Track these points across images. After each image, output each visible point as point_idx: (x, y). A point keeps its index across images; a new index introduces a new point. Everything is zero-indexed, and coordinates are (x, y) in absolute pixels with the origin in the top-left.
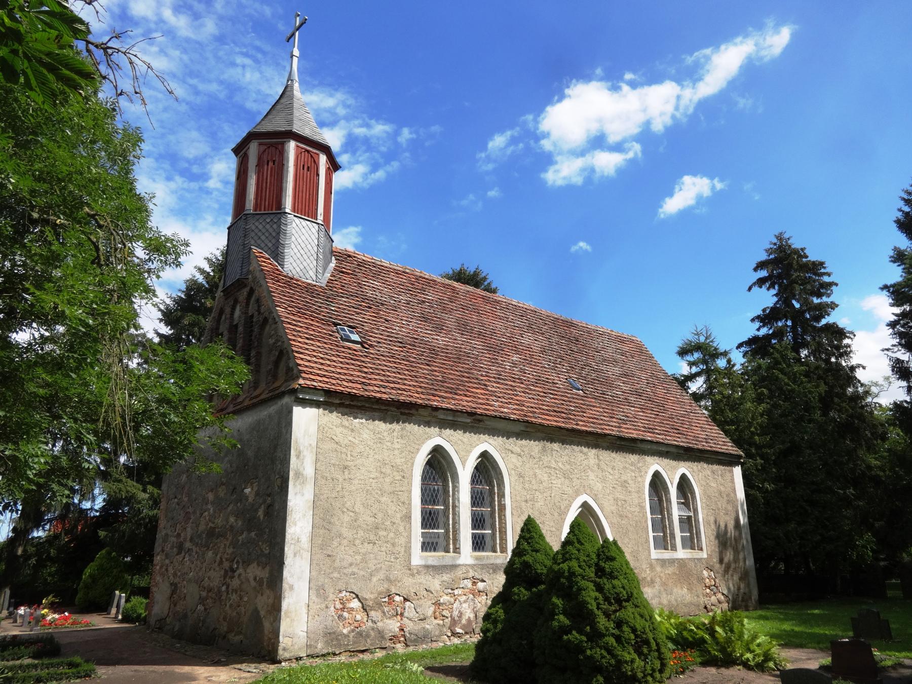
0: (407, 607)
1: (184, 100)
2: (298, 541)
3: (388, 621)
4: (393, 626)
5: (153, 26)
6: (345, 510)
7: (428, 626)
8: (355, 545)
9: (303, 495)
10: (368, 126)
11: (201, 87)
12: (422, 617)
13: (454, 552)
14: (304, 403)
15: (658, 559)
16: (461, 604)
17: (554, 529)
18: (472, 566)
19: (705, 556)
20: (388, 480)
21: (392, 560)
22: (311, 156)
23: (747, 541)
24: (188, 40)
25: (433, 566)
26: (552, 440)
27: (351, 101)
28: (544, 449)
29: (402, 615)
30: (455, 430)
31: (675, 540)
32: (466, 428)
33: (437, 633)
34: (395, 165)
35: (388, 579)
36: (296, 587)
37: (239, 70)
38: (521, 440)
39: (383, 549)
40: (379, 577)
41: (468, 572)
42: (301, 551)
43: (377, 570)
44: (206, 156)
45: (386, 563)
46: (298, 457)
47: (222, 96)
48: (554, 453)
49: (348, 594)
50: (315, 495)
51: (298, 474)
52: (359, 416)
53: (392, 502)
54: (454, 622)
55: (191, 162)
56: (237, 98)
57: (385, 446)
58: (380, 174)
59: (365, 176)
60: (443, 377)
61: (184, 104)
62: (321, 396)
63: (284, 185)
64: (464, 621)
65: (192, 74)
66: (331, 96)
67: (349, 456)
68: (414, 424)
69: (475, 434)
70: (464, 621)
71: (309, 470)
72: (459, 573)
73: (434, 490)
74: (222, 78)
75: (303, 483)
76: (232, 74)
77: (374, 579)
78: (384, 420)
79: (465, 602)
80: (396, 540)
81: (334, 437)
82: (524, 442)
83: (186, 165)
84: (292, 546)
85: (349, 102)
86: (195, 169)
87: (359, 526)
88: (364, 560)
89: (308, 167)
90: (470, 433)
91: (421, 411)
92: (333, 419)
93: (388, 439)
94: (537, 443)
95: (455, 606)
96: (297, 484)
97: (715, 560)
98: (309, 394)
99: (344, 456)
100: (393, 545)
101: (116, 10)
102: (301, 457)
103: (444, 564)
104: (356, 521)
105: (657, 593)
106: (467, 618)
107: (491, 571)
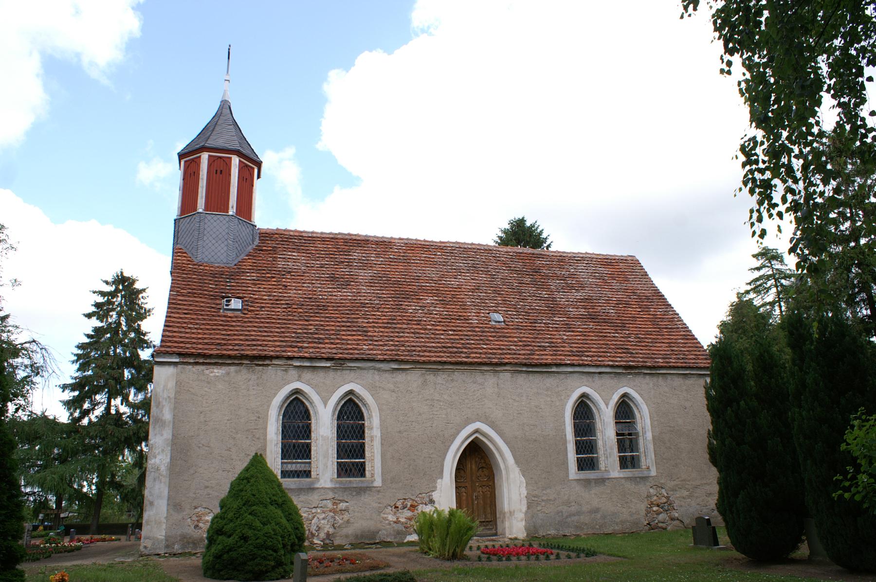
2: (158, 469)
9: (162, 435)
15: (579, 480)
22: (224, 160)
36: (156, 503)
42: (161, 477)
49: (203, 510)
50: (173, 435)
53: (247, 438)
57: (240, 394)
71: (167, 415)
73: (299, 427)
75: (162, 426)
79: (324, 519)
84: (153, 473)
89: (221, 171)
95: (313, 521)
96: (157, 426)
102: (160, 407)
104: (211, 454)
105: (235, 543)
106: (326, 532)
107: (354, 493)
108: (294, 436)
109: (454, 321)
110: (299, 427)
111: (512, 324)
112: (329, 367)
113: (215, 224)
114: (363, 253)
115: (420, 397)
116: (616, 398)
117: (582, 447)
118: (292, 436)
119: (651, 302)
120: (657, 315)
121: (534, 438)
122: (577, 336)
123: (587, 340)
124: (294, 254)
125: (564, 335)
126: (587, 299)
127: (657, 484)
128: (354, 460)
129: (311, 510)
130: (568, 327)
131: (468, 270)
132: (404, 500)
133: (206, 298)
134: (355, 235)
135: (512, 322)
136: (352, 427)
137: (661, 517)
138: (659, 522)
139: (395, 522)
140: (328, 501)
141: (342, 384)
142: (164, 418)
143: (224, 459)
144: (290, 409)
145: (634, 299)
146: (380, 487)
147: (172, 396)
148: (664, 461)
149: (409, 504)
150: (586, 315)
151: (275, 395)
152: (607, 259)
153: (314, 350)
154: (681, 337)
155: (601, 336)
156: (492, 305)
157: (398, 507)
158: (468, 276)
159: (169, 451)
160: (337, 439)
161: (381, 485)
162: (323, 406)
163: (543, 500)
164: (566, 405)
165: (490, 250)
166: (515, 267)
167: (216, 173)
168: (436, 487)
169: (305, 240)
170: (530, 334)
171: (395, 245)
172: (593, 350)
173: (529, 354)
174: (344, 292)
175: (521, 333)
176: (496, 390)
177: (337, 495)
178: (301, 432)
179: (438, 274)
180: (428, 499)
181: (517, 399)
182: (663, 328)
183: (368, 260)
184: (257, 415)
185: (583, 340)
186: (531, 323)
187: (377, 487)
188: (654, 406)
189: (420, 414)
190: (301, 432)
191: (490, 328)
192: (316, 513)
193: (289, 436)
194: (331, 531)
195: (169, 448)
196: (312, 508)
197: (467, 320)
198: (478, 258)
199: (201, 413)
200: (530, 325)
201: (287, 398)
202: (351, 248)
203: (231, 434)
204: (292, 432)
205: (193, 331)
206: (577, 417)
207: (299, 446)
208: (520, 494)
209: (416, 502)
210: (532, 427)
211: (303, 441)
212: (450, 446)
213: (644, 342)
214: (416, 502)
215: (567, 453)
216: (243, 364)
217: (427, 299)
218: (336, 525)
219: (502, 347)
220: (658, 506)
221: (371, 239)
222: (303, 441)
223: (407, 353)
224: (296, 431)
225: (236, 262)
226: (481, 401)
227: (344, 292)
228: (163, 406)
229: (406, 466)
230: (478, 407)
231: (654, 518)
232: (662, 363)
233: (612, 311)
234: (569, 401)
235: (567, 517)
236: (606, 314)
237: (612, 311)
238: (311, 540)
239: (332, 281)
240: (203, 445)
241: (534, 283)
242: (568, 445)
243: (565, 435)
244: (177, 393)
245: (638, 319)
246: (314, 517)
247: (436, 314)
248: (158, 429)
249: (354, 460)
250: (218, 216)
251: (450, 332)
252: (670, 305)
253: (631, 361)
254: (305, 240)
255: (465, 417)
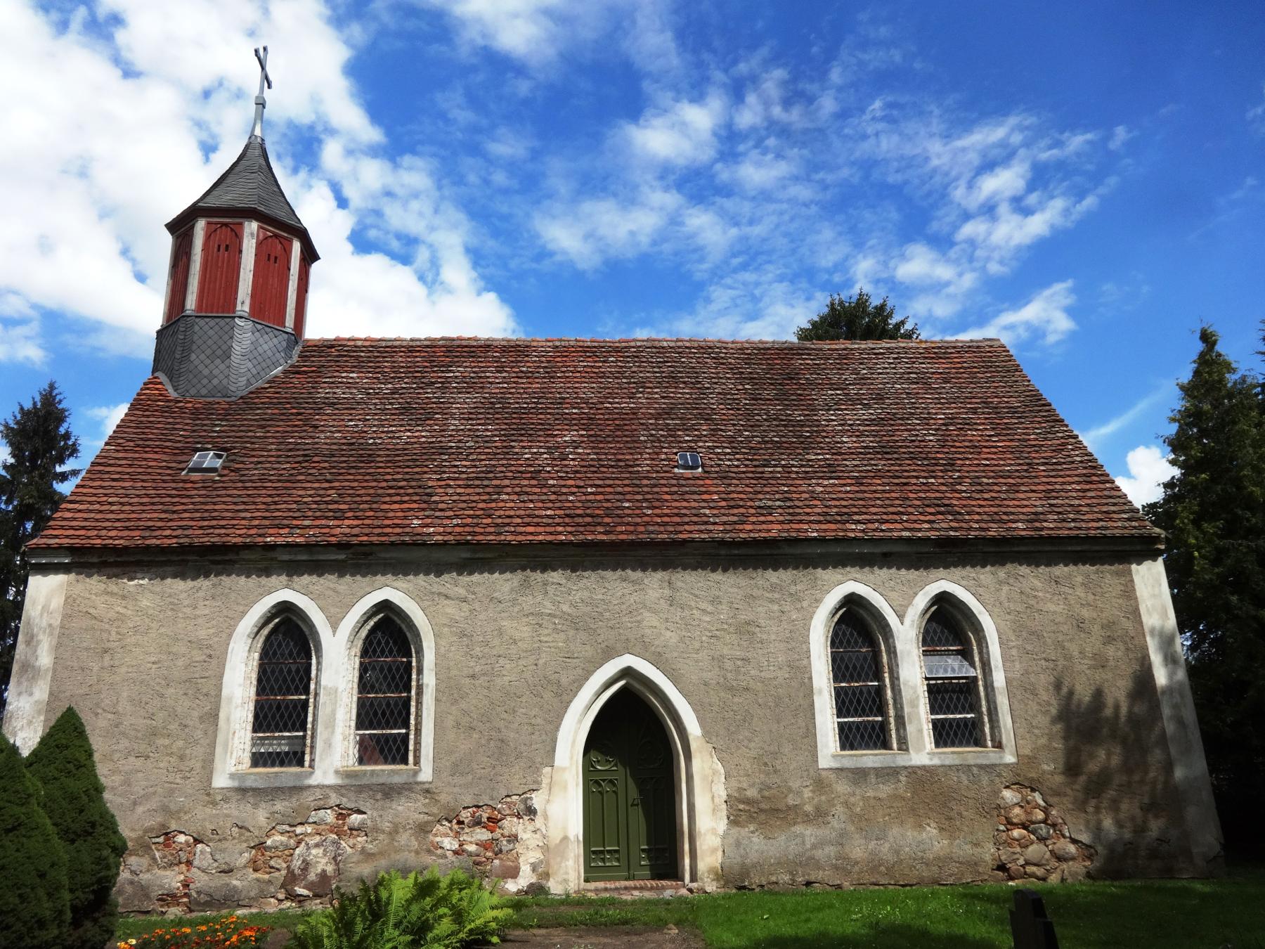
0: (198, 851)
1: (812, 202)
3: (161, 873)
4: (172, 879)
5: (763, 133)
6: (100, 711)
7: (235, 882)
8: (112, 760)
9: (31, 694)
10: (1058, 144)
11: (830, 178)
12: (224, 867)
13: (899, 749)
14: (44, 569)
15: (841, 770)
16: (308, 848)
17: (539, 721)
18: (336, 788)
19: (1010, 758)
20: (180, 663)
21: (178, 781)
22: (232, 230)
23: (1180, 722)
24: (806, 131)
25: (254, 790)
26: (545, 567)
27: (1031, 120)
28: (525, 584)
29: (189, 863)
30: (320, 575)
31: (905, 729)
32: (341, 569)
33: (252, 894)
34: (1113, 181)
35: (165, 809)
37: (872, 141)
38: (471, 573)
39: (161, 765)
40: (148, 806)
41: (327, 797)
43: (147, 797)
44: (846, 258)
45: (166, 785)
46: (28, 643)
47: (856, 180)
48: (551, 589)
50: (51, 694)
51: (26, 667)
52: (139, 575)
54: (291, 878)
55: (830, 272)
56: (876, 175)
57: (180, 615)
58: (1090, 202)
59: (1066, 212)
60: (339, 495)
61: (813, 206)
62: (66, 557)
63: (170, 282)
64: (312, 876)
65: (816, 168)
66: (1000, 124)
67: (113, 633)
68: (238, 575)
69: (364, 576)
70: (312, 876)
71: (45, 659)
72: (309, 799)
73: (289, 671)
74: (852, 158)
75: (33, 678)
76: (866, 147)
77: (140, 809)
78: (183, 576)
79: (317, 845)
80: (188, 752)
81: (91, 611)
82: (476, 577)
83: (826, 277)
85: (1027, 123)
86: (837, 278)
87: (124, 734)
88: (127, 783)
89: (227, 246)
90: (353, 575)
91: (246, 555)
92: (93, 588)
93: (186, 602)
94: (508, 575)
95: (298, 851)
96: (23, 680)
97: (1049, 767)
98: (44, 556)
99: (105, 636)
100: (182, 758)
101: (723, 133)
103: (277, 785)
104: (117, 726)
107: (379, 796)
108: (280, 689)
109: (605, 470)
110: (289, 671)
111: (717, 469)
112: (343, 561)
113: (211, 332)
114: (475, 367)
115: (516, 610)
116: (922, 600)
117: (851, 702)
118: (276, 688)
119: (1020, 417)
120: (1029, 440)
121: (744, 684)
122: (845, 485)
123: (865, 492)
124: (351, 375)
125: (818, 485)
126: (882, 419)
127: (1020, 779)
128: (389, 731)
129: (293, 829)
130: (831, 470)
131: (659, 382)
132: (475, 809)
133: (165, 453)
134: (469, 339)
135: (719, 465)
136: (390, 669)
137: (1035, 850)
138: (1027, 863)
139: (456, 852)
140: (329, 811)
141: (368, 589)
142: (37, 664)
143: (139, 735)
144: (276, 640)
145: (983, 413)
146: (430, 783)
147: (57, 622)
148: (1036, 731)
149: (485, 816)
150: (874, 447)
151: (244, 613)
152: (940, 348)
153: (317, 531)
154: (1077, 479)
155: (897, 484)
156: (687, 438)
157: (462, 823)
158: (656, 393)
159: (42, 724)
160: (360, 692)
161: (430, 780)
162: (330, 631)
163: (761, 810)
164: (812, 618)
165: (710, 348)
166: (751, 373)
167: (219, 250)
168: (539, 783)
169: (378, 352)
170: (747, 486)
171: (535, 351)
172: (873, 510)
173: (735, 523)
174: (417, 431)
175: (730, 485)
176: (667, 592)
177: (344, 800)
178: (293, 680)
179: (600, 393)
180: (522, 807)
181: (710, 609)
182: (1038, 464)
183: (481, 377)
184: (208, 652)
185: (857, 492)
186: (755, 466)
187: (424, 783)
188: (1008, 617)
189: (515, 642)
190: (293, 680)
191: (672, 478)
192: (306, 834)
193: (272, 689)
194: (330, 869)
195: (42, 718)
196: (295, 826)
197: (631, 466)
198: (683, 362)
199: (106, 652)
200: (753, 469)
201: (267, 620)
202: (456, 359)
203: (157, 688)
204: (277, 680)
205: (114, 508)
206: (841, 643)
207: (287, 707)
208: (713, 797)
209: (499, 812)
210: (739, 663)
211: (296, 697)
212: (571, 701)
213: (991, 491)
214: (499, 812)
215: (813, 714)
216: (188, 561)
217: (565, 436)
218: (339, 858)
219: (683, 511)
220: (1025, 827)
221: (495, 343)
222: (296, 697)
223: (492, 530)
224: (285, 680)
225: (244, 393)
226: (635, 613)
227: (417, 431)
228: (38, 642)
229: (483, 742)
230: (629, 625)
231: (1014, 853)
232: (1024, 529)
233: (931, 438)
234: (819, 611)
235: (814, 847)
236: (917, 444)
237: (931, 438)
238: (289, 887)
239: (402, 414)
240: (104, 710)
241: (782, 397)
242: (816, 698)
243: (810, 678)
244: (67, 617)
245: (984, 450)
246: (299, 843)
247: (573, 460)
248: (25, 684)
249: (389, 731)
250: (217, 320)
251: (589, 490)
252: (1062, 421)
253: (952, 529)
254: (378, 352)
255: (603, 646)
